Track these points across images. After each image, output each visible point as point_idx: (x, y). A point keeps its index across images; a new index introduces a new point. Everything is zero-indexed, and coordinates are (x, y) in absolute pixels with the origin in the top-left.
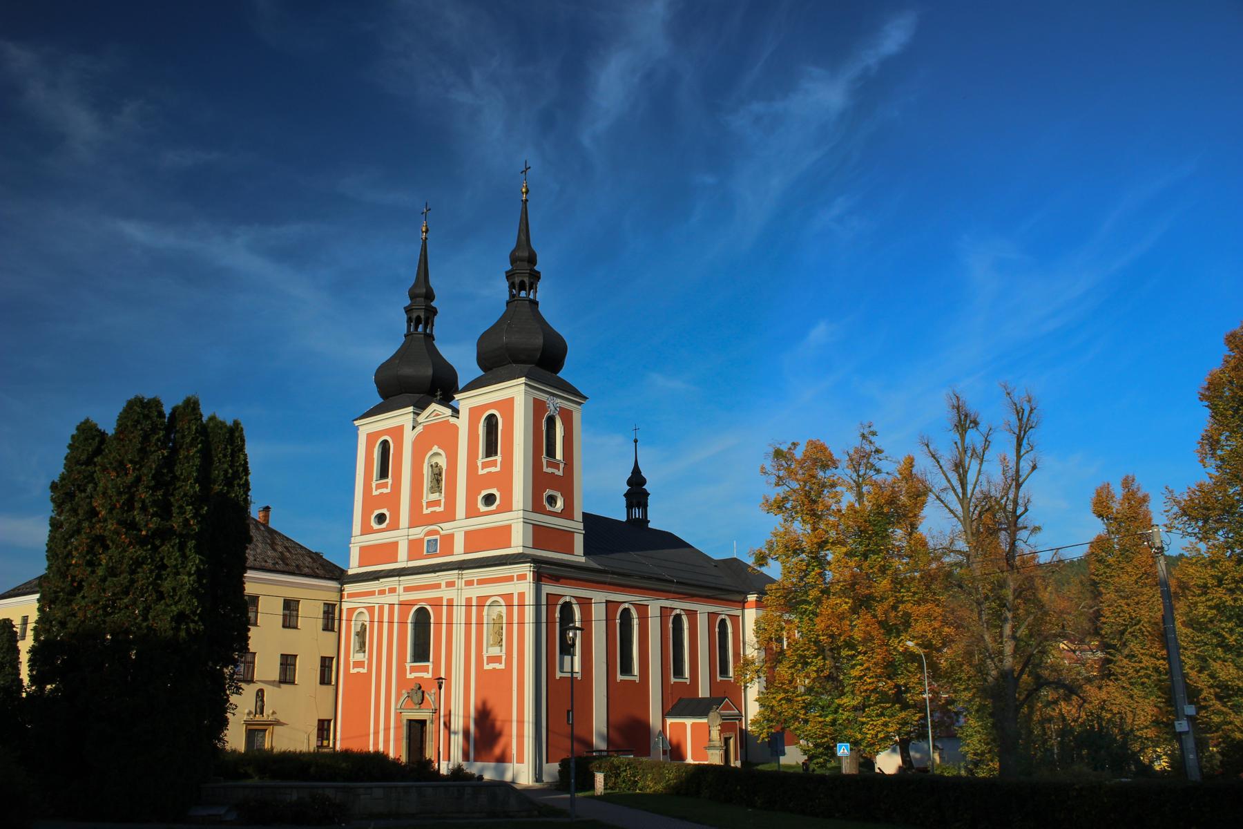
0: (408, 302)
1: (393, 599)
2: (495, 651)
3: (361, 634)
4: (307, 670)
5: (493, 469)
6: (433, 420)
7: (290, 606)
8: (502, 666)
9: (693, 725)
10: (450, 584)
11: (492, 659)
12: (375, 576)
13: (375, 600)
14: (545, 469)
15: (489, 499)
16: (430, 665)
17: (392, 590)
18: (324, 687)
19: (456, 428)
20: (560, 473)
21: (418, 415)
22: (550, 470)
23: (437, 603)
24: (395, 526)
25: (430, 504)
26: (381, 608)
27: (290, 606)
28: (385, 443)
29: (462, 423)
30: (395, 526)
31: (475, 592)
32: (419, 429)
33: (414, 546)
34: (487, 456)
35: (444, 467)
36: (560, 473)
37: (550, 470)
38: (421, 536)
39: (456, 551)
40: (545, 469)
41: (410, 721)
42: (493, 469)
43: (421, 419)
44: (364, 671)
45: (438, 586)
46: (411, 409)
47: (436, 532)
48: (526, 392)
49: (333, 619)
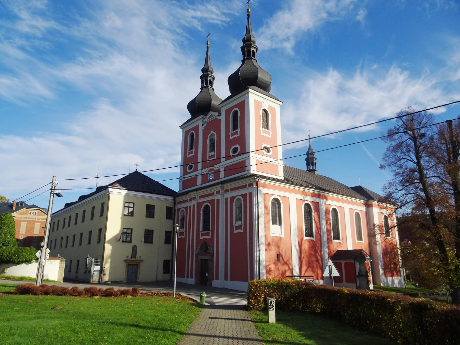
0: (201, 74)
1: (194, 202)
2: (239, 223)
3: (182, 220)
4: (159, 237)
5: (236, 136)
6: (212, 119)
7: (30, 213)
8: (242, 231)
9: (345, 264)
10: (218, 192)
11: (238, 227)
12: (187, 193)
13: (187, 205)
14: (262, 134)
15: (235, 150)
16: (210, 232)
17: (194, 198)
18: (167, 245)
19: (220, 120)
20: (270, 137)
21: (204, 118)
22: (265, 135)
23: (212, 202)
24: (196, 170)
25: (210, 157)
26: (190, 207)
27: (30, 213)
28: (192, 135)
29: (223, 118)
30: (196, 170)
31: (229, 195)
32: (205, 124)
33: (204, 176)
34: (234, 130)
35: (216, 139)
36: (270, 137)
37: (265, 135)
38: (207, 172)
39: (221, 177)
40: (262, 134)
41: (201, 260)
42: (236, 136)
43: (206, 120)
44: (183, 237)
45: (213, 194)
46: (201, 116)
47: (213, 170)
48: (306, 147)
49: (172, 214)
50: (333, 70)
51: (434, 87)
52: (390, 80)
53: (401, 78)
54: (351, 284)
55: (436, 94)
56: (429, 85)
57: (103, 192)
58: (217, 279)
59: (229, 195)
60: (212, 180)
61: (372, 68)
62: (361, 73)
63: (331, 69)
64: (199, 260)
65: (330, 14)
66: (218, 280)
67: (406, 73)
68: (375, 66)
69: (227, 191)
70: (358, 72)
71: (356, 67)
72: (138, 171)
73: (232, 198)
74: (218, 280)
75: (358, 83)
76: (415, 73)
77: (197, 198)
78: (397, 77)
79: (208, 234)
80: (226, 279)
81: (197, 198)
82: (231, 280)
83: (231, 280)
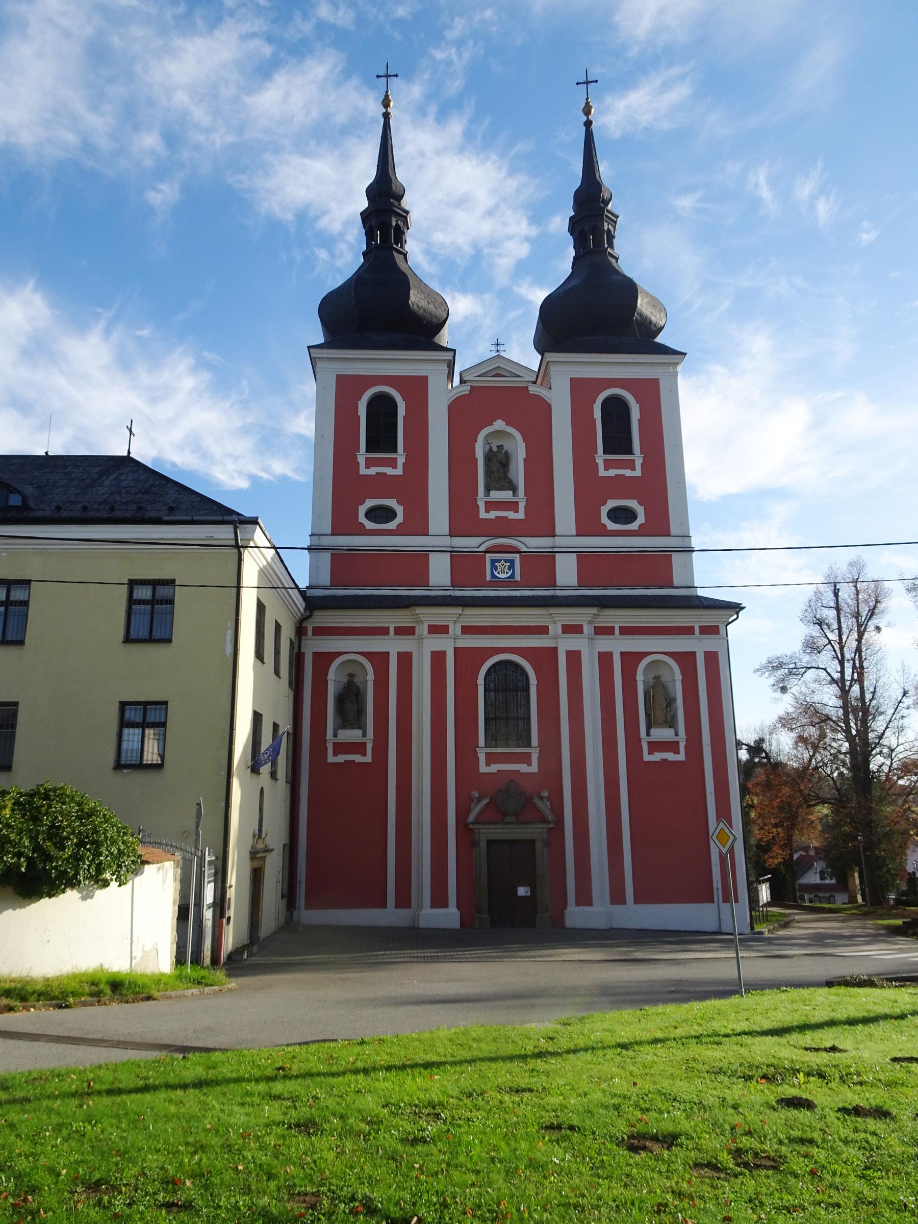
19: (546, 408)
31: (617, 646)
50: (35, 289)
51: (245, 431)
52: (166, 376)
53: (189, 383)
54: (608, 892)
55: (244, 445)
56: (238, 424)
57: (224, 533)
58: (585, 898)
59: (617, 646)
60: (509, 583)
61: (138, 333)
62: (107, 332)
63: (31, 284)
64: (483, 844)
65: (88, 147)
66: (589, 903)
67: (207, 376)
68: (146, 332)
69: (607, 631)
70: (102, 324)
71: (99, 310)
72: (50, 454)
73: (631, 660)
74: (589, 903)
75: (90, 351)
76: (221, 384)
77: (455, 630)
78: (182, 376)
79: (359, 748)
80: (617, 897)
81: (455, 630)
82: (637, 901)
83: (637, 901)
